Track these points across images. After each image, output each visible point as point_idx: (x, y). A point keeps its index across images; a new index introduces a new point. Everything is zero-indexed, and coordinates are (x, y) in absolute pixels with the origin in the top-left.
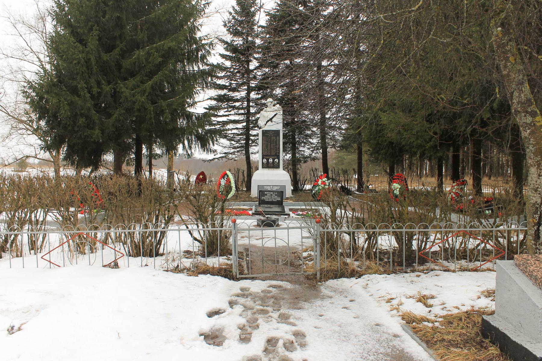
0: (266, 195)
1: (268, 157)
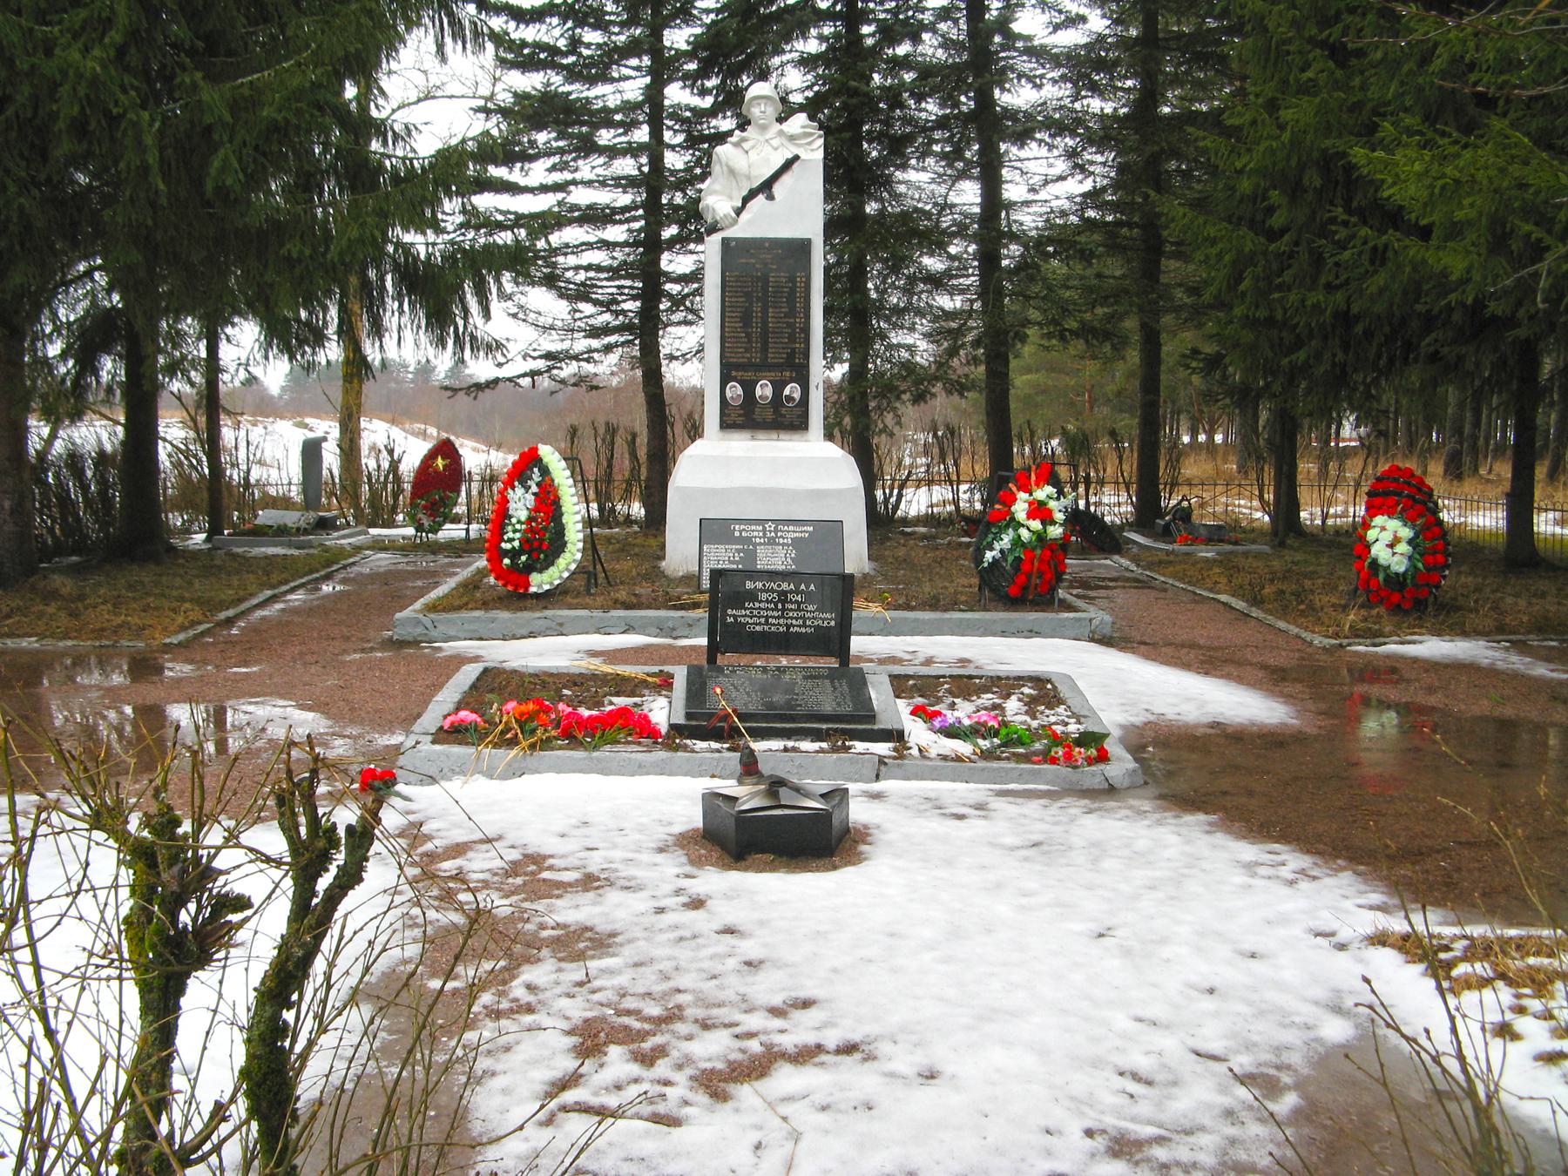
0: (752, 596)
1: (749, 375)
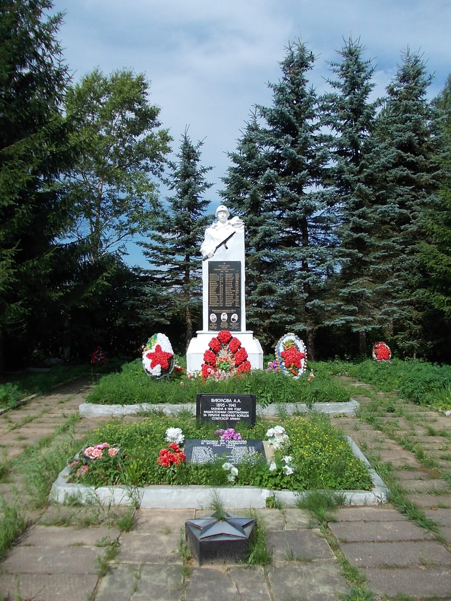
0: (214, 405)
1: (219, 311)
